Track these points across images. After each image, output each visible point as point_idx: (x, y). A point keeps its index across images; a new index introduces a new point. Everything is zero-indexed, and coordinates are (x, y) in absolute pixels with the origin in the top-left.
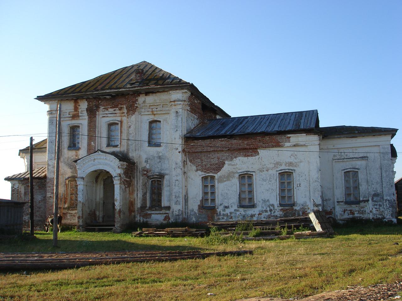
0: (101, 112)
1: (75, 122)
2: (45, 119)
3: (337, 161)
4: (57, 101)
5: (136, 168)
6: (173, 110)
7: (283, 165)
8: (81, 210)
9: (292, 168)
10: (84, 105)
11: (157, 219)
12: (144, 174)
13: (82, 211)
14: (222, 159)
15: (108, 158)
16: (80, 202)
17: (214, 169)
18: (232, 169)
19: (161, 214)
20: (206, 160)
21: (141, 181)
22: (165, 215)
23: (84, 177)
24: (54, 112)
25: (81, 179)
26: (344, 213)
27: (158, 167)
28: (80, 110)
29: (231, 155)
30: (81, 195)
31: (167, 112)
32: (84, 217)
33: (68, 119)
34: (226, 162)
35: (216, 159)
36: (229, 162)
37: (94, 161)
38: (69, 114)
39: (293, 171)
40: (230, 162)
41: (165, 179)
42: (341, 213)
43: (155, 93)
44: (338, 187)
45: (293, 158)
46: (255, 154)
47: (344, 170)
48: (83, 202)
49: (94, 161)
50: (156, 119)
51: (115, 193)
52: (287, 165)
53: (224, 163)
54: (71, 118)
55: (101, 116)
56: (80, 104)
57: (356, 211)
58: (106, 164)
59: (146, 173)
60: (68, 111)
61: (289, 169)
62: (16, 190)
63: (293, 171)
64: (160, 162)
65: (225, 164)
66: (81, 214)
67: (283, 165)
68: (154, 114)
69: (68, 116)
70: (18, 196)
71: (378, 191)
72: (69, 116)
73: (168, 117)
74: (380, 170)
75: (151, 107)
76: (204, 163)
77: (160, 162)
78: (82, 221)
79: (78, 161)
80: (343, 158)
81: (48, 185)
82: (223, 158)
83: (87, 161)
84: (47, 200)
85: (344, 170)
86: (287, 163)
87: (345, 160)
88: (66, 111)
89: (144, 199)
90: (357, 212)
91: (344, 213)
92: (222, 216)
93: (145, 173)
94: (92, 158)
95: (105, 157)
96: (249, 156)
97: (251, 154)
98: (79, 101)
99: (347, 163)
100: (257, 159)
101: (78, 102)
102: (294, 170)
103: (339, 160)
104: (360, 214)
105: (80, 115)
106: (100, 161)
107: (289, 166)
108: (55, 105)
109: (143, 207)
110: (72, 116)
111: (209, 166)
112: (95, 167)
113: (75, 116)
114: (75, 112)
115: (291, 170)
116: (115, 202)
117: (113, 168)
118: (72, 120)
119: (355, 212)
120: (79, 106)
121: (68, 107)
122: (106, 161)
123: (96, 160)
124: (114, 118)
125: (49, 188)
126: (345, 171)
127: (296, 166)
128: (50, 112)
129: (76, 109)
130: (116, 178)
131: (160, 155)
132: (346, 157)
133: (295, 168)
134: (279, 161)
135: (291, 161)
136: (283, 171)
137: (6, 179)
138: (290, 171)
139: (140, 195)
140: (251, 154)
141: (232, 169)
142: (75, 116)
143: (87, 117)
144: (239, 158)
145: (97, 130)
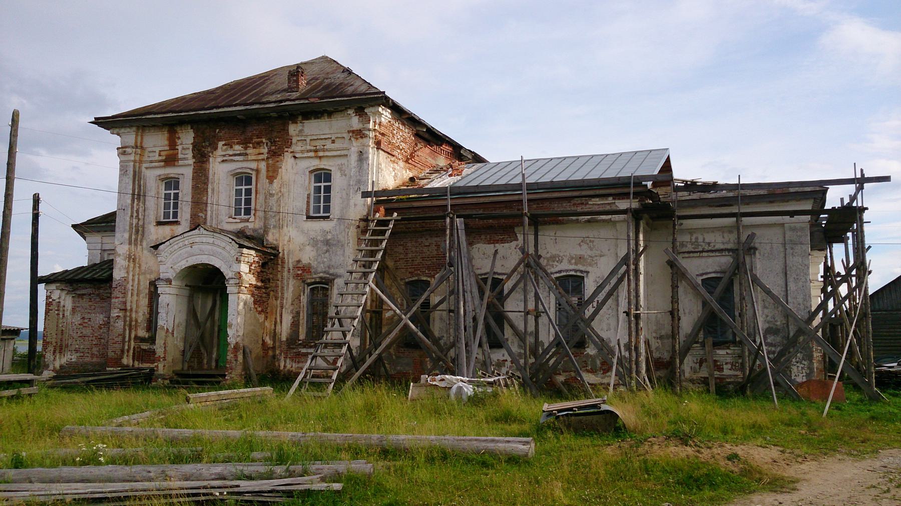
0: (219, 152)
1: (171, 171)
2: (114, 161)
3: (687, 255)
4: (134, 129)
5: (280, 262)
6: (143, 169)
7: (565, 261)
9: (583, 269)
10: (187, 138)
12: (298, 275)
17: (428, 268)
20: (414, 249)
21: (291, 289)
24: (129, 150)
26: (700, 366)
27: (324, 263)
28: (180, 148)
31: (343, 153)
32: (169, 359)
33: (156, 164)
35: (434, 247)
38: (160, 155)
39: (585, 275)
41: (335, 287)
42: (693, 365)
43: (330, 114)
44: (687, 311)
45: (585, 246)
47: (702, 275)
50: (322, 167)
51: (11, 262)
52: (573, 261)
54: (162, 164)
55: (220, 159)
56: (180, 135)
57: (727, 364)
59: (302, 271)
60: (157, 150)
61: (576, 271)
62: (54, 303)
63: (585, 275)
64: (327, 251)
67: (565, 261)
68: (320, 157)
69: (157, 158)
70: (58, 314)
71: (778, 323)
72: (160, 158)
73: (346, 163)
74: (782, 275)
75: (314, 143)
76: (410, 256)
77: (327, 251)
79: (161, 247)
80: (700, 249)
81: (116, 293)
83: (176, 247)
84: (112, 323)
85: (702, 275)
86: (572, 258)
87: (705, 254)
88: (154, 149)
89: (295, 324)
90: (729, 366)
91: (700, 366)
93: (299, 272)
98: (178, 129)
99: (710, 260)
100: (513, 248)
101: (176, 132)
102: (588, 272)
103: (691, 255)
104: (735, 370)
105: (180, 156)
106: (203, 247)
107: (576, 264)
108: (131, 137)
109: (293, 340)
110: (164, 158)
111: (419, 260)
112: (194, 258)
113: (171, 160)
114: (171, 152)
115: (581, 271)
118: (164, 167)
119: (725, 367)
120: (179, 138)
121: (156, 142)
124: (245, 165)
125: (117, 300)
126: (705, 277)
127: (590, 265)
128: (122, 151)
129: (173, 145)
131: (329, 237)
132: (707, 248)
133: (589, 269)
134: (558, 253)
135: (582, 253)
136: (564, 274)
138: (579, 274)
139: (287, 319)
142: (171, 160)
143: (191, 161)
144: (478, 245)
145: (210, 186)
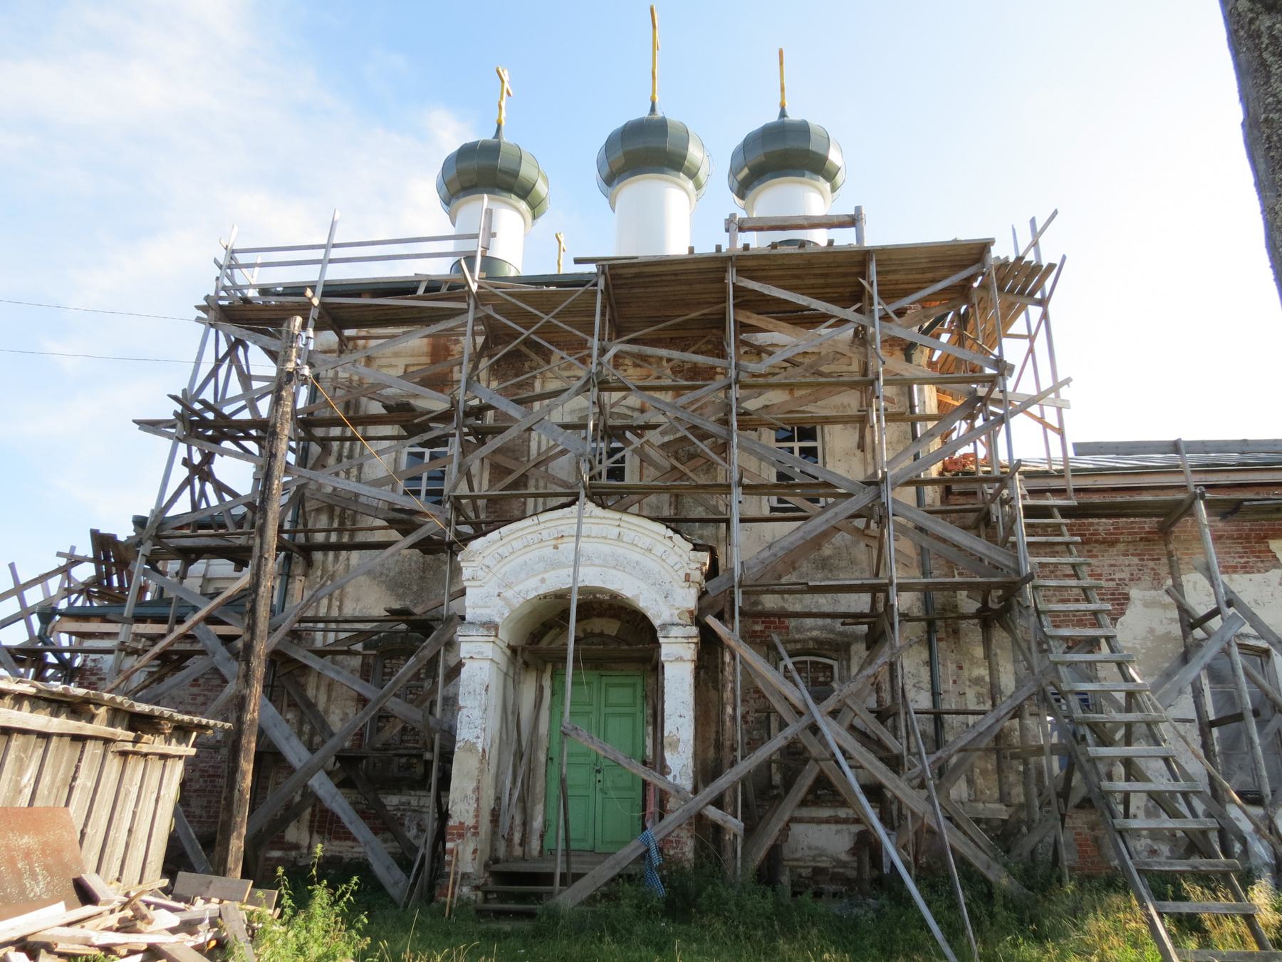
8: (470, 793)
11: (816, 848)
13: (478, 800)
14: (1113, 580)
15: (629, 535)
16: (471, 747)
18: (1165, 621)
19: (838, 821)
22: (855, 829)
23: (497, 620)
25: (483, 631)
29: (1151, 564)
30: (477, 713)
34: (1134, 593)
36: (1147, 593)
37: (556, 547)
40: (1153, 592)
46: (1260, 565)
48: (484, 751)
49: (556, 547)
53: (1127, 598)
58: (618, 565)
65: (1128, 599)
66: (472, 814)
78: (475, 851)
82: (1117, 576)
92: (1149, 841)
94: (544, 532)
95: (617, 530)
96: (1235, 572)
97: (1242, 561)
116: (667, 754)
117: (654, 584)
122: (621, 550)
123: (565, 540)
130: (675, 631)
137: (134, 421)
140: (1242, 561)
141: (1165, 621)
